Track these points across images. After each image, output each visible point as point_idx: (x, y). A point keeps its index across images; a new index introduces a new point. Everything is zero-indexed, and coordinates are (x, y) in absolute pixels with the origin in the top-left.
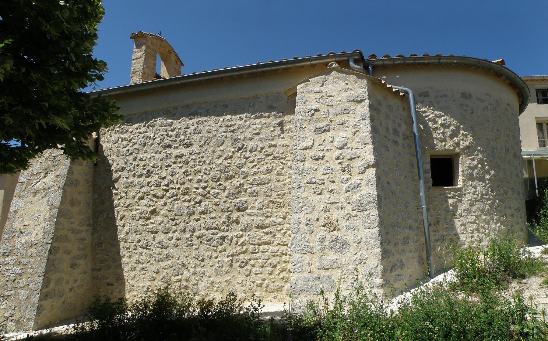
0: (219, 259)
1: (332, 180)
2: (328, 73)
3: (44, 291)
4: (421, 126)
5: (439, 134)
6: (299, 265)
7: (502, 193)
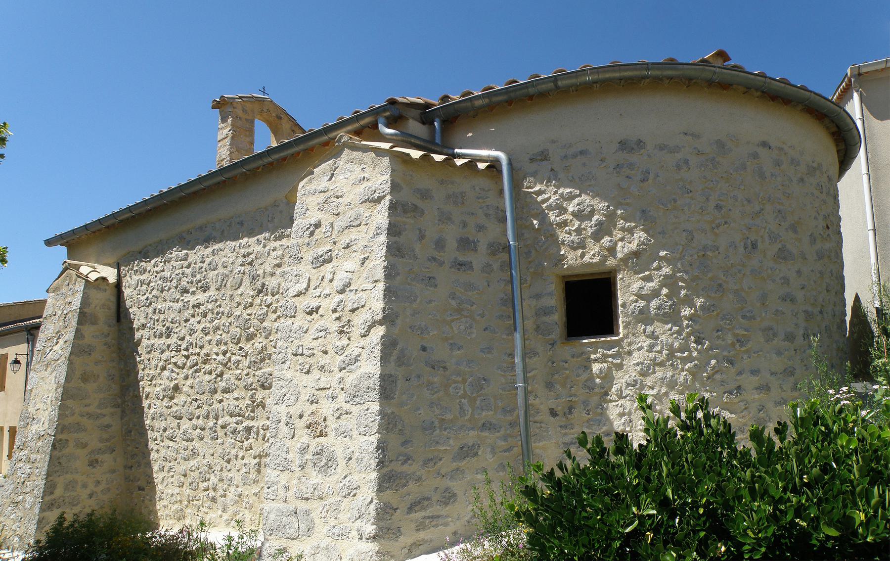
0: (246, 461)
1: (323, 349)
2: (337, 154)
3: (47, 498)
4: (535, 222)
5: (570, 233)
6: (273, 488)
7: (730, 342)
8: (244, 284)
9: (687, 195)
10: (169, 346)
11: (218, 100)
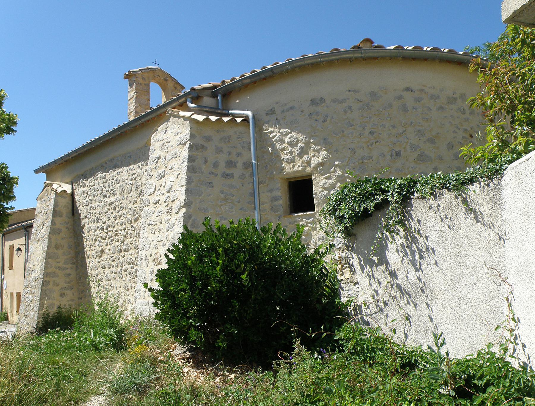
2: (168, 120)
3: (40, 312)
4: (270, 149)
5: (287, 155)
8: (132, 191)
9: (350, 128)
10: (98, 227)
11: (127, 73)
